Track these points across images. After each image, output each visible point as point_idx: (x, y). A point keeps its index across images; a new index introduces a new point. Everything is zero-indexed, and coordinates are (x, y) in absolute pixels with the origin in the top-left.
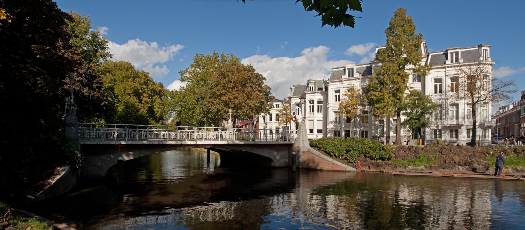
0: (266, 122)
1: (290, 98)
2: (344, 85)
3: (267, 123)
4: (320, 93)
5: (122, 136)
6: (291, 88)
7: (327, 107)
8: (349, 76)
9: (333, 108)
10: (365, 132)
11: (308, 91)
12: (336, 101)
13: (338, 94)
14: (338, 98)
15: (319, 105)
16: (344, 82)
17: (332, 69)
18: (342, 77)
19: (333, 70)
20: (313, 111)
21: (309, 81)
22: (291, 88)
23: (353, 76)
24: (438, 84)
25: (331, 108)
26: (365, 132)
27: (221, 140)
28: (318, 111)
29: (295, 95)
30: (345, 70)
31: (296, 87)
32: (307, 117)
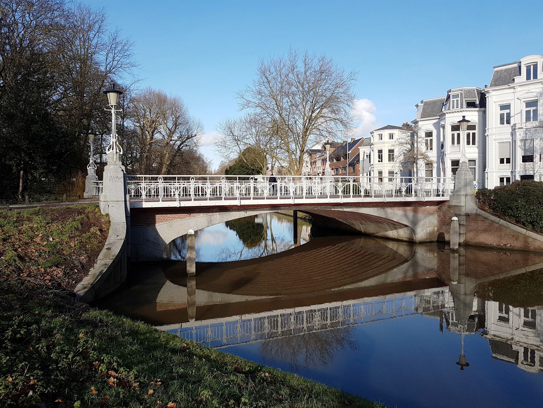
0: (372, 163)
1: (416, 122)
2: (517, 95)
3: (374, 166)
4: (124, 173)
5: (171, 192)
6: (417, 106)
7: (486, 134)
8: (528, 78)
9: (498, 137)
10: (507, 178)
11: (449, 109)
12: (390, 139)
13: (508, 111)
14: (505, 119)
15: (453, 132)
16: (519, 89)
17: (494, 68)
18: (514, 80)
19: (496, 69)
20: (459, 142)
21: (450, 91)
22: (417, 106)
23: (535, 77)
24: (532, 109)
25: (494, 136)
26: (507, 178)
27: (353, 197)
28: (468, 143)
29: (425, 115)
30: (520, 67)
31: (426, 104)
32: (449, 154)
